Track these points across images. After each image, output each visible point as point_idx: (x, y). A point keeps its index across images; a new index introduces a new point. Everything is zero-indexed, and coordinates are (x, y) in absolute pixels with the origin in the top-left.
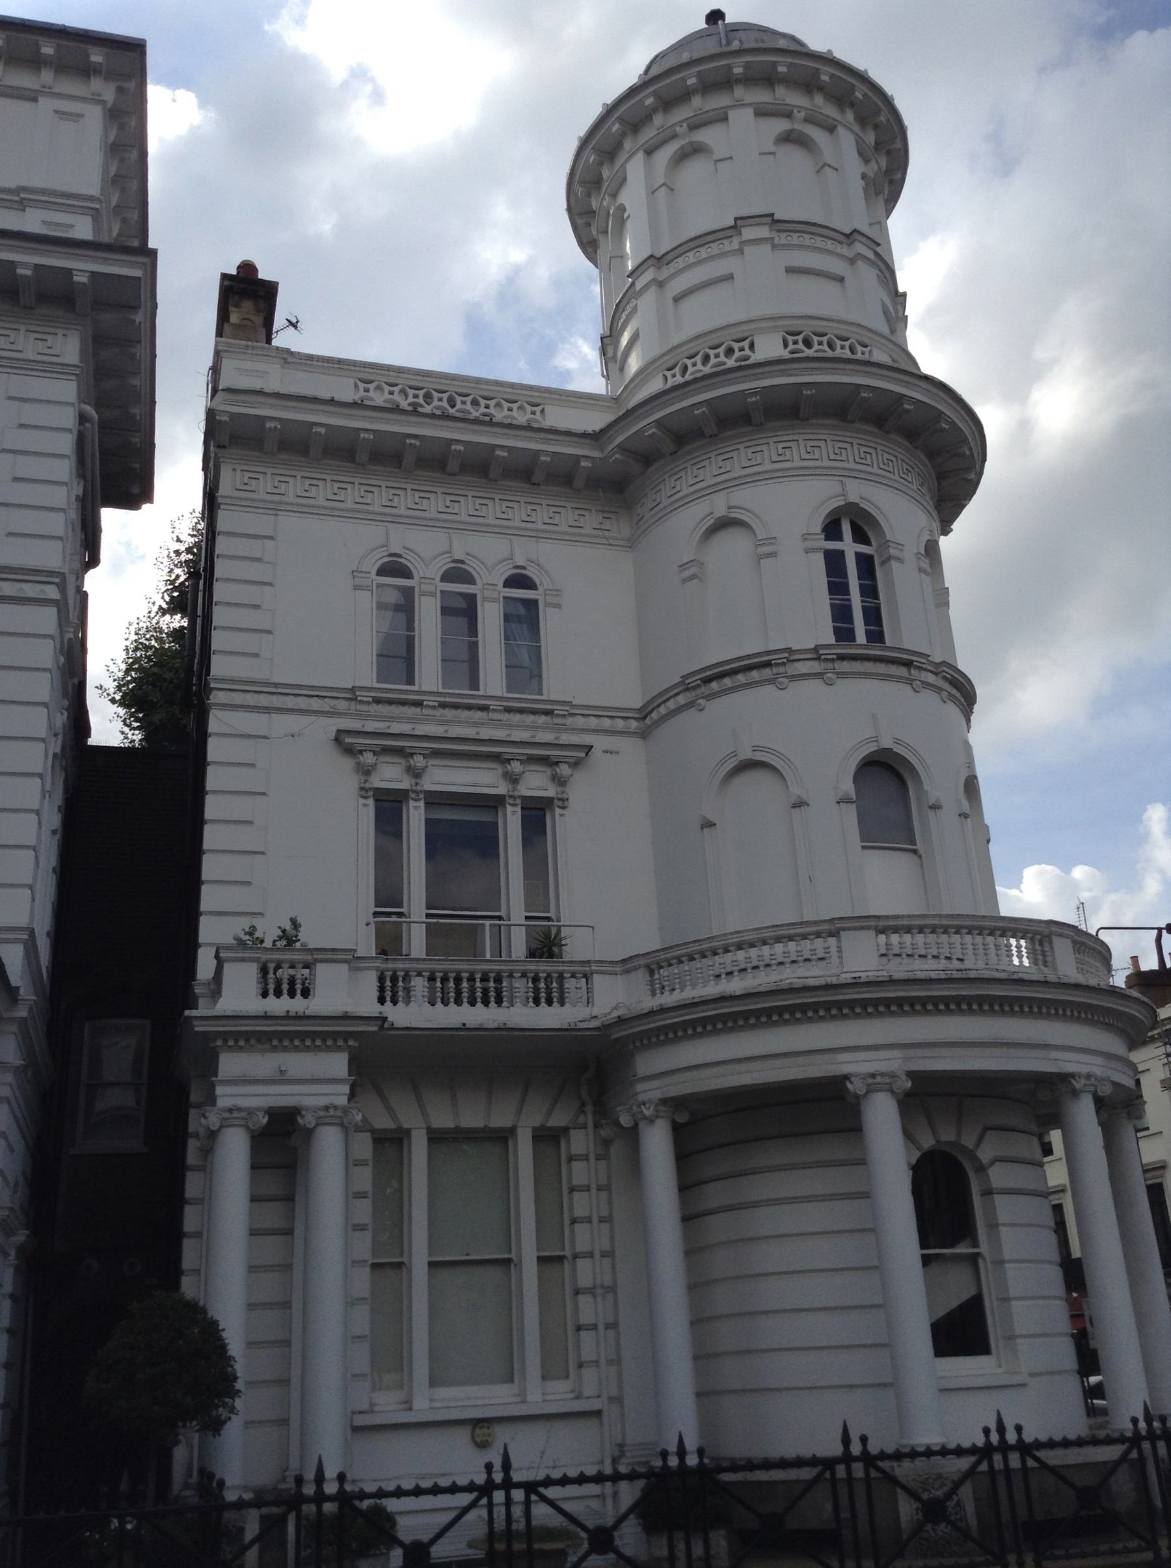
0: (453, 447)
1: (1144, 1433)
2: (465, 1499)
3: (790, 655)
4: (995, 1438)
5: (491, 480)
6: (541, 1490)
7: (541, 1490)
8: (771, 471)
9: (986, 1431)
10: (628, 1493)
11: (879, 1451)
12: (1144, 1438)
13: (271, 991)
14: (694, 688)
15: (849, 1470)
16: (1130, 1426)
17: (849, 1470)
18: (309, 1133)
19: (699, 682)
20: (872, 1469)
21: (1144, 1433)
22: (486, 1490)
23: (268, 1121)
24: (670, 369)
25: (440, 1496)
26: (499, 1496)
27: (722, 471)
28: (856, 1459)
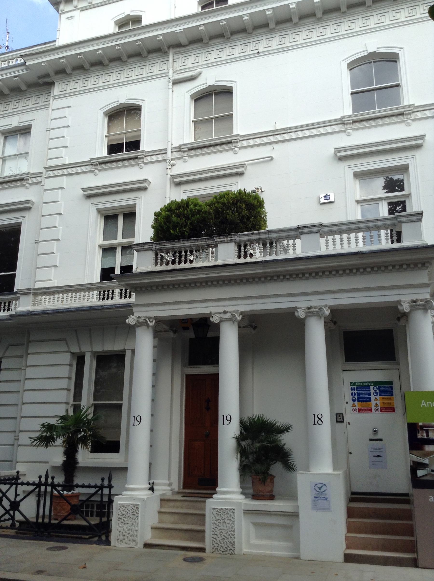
0: (267, 13)
1: (43, 482)
2: (31, 488)
3: (414, 109)
4: (43, 480)
5: (145, 57)
6: (57, 487)
7: (57, 487)
8: (344, 34)
9: (40, 477)
10: (106, 499)
11: (27, 482)
12: (43, 485)
13: (242, 256)
14: (95, 165)
15: (46, 489)
16: (38, 479)
17: (46, 489)
18: (217, 327)
19: (97, 163)
20: (54, 490)
21: (43, 482)
22: (39, 485)
23: (242, 319)
24: (4, 62)
25: (24, 486)
26: (43, 488)
27: (350, 28)
28: (49, 485)
